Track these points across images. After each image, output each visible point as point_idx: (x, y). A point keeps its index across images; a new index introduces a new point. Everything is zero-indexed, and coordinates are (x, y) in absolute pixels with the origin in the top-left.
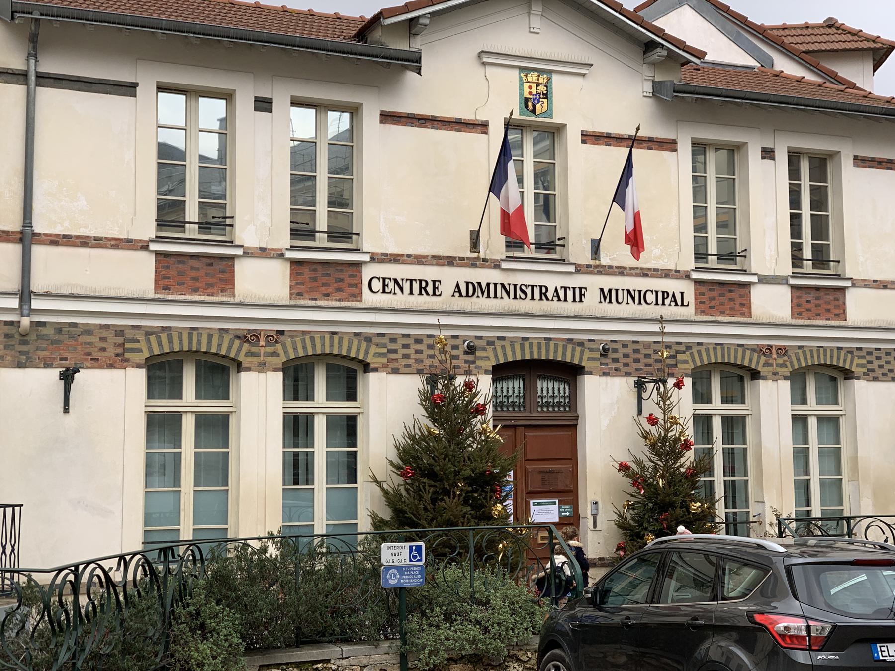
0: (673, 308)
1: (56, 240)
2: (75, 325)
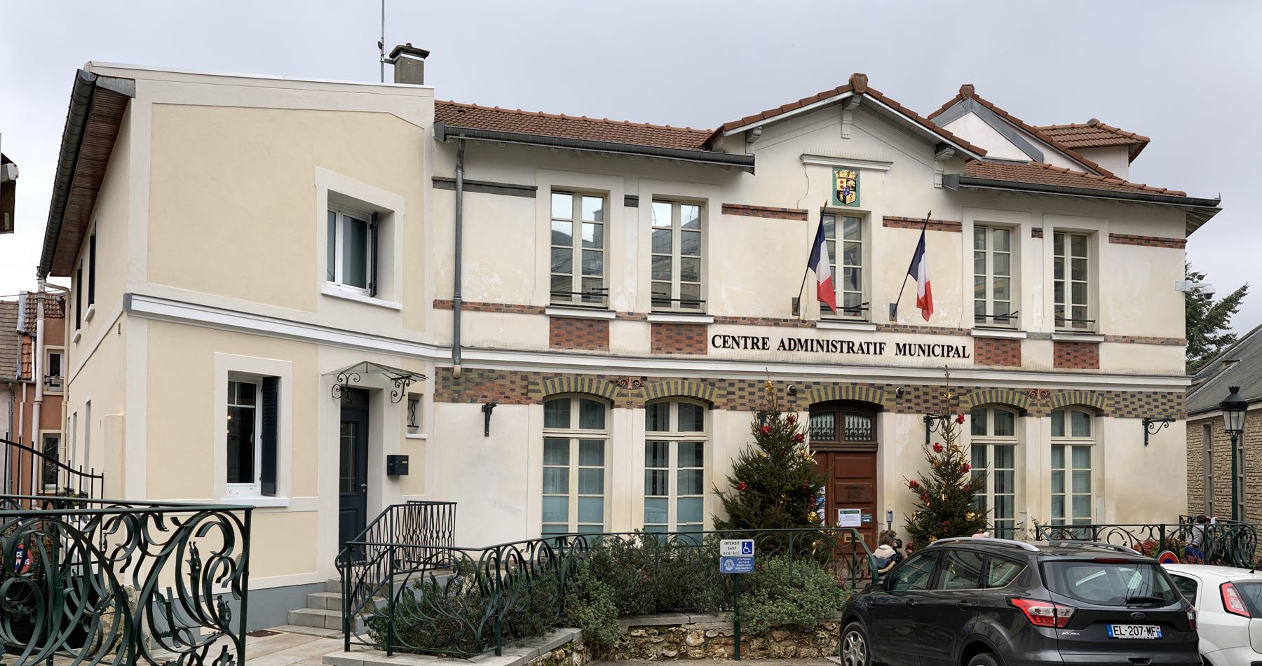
0: (956, 359)
2: (492, 371)
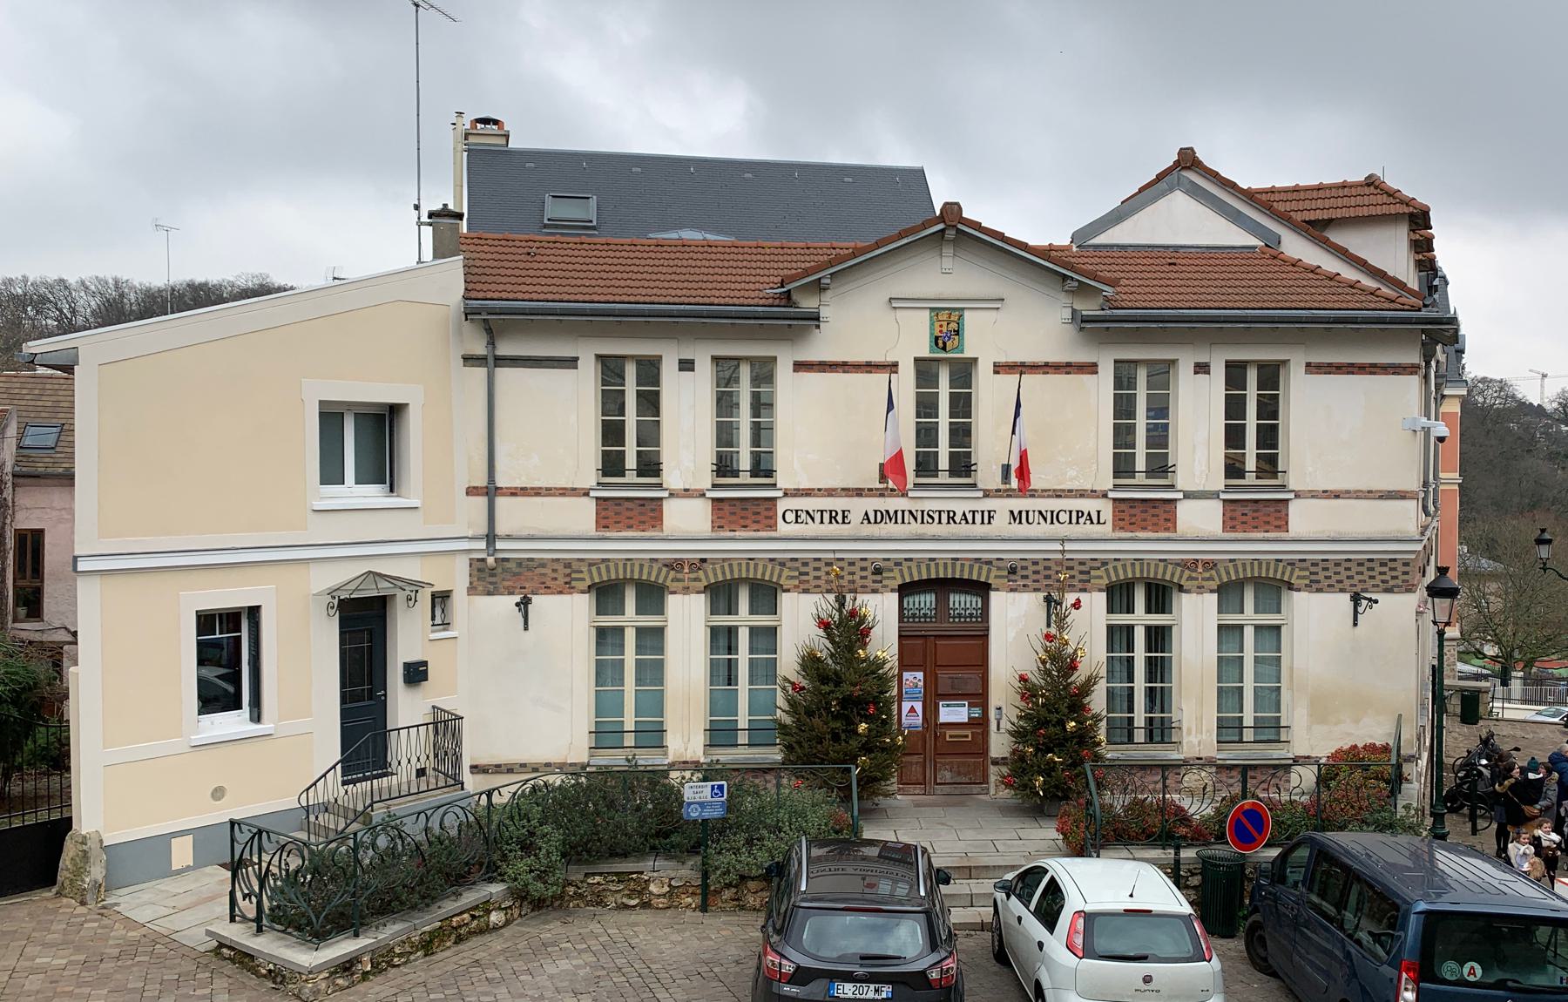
1: (514, 493)
2: (532, 560)
